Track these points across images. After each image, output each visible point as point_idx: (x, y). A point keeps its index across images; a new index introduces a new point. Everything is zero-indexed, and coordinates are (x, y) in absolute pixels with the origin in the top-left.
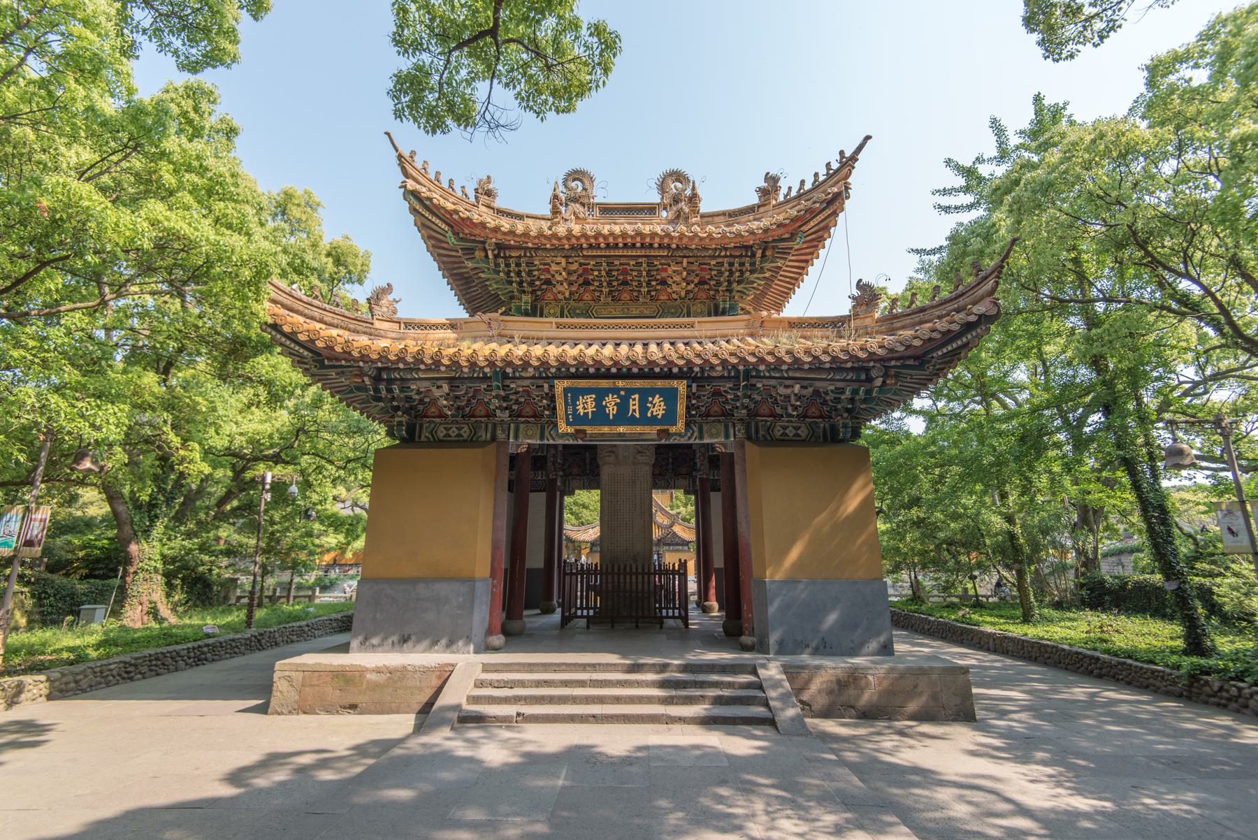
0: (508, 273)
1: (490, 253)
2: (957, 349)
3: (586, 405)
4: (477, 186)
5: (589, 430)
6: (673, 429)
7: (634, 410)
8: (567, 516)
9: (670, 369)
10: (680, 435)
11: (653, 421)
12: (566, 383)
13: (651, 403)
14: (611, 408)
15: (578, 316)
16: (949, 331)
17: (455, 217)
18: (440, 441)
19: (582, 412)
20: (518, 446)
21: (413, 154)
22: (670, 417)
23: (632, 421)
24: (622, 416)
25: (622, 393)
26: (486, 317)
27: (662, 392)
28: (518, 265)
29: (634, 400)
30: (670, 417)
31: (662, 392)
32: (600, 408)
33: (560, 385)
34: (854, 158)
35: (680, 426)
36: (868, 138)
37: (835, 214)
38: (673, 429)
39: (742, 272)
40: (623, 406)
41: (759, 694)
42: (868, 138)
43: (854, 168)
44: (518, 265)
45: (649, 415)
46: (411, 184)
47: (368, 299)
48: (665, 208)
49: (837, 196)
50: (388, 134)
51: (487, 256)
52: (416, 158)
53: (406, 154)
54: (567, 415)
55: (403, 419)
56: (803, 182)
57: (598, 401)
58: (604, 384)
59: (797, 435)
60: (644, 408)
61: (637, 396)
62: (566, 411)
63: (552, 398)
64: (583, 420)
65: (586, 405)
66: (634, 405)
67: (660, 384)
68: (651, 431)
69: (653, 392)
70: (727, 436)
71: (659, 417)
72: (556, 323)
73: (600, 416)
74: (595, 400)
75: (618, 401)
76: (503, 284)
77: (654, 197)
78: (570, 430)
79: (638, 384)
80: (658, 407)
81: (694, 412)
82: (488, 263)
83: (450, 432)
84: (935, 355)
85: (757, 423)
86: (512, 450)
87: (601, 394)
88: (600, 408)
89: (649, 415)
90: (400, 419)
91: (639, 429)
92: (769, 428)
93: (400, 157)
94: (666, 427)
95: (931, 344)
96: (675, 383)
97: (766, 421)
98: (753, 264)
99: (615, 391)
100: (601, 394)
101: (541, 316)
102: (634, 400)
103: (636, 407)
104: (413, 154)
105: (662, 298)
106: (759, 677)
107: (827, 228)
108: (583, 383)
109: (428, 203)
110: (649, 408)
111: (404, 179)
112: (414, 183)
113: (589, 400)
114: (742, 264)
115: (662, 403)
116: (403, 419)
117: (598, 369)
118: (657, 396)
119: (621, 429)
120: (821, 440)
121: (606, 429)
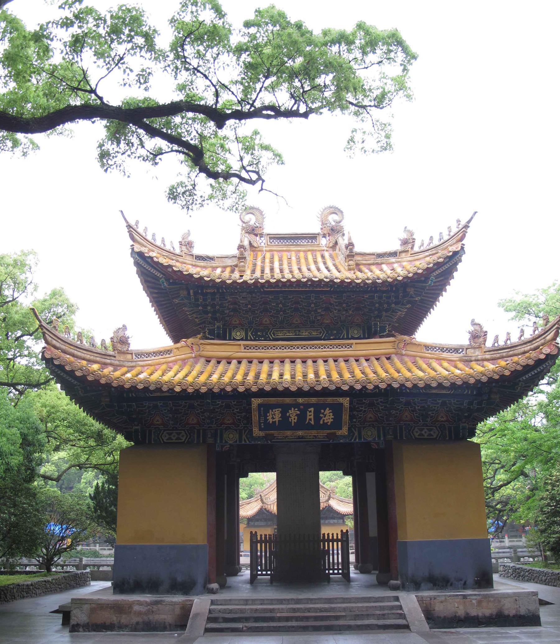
0: (205, 306)
1: (191, 292)
2: (536, 374)
3: (275, 416)
4: (181, 240)
5: (275, 433)
6: (339, 433)
7: (310, 419)
10: (344, 437)
11: (325, 426)
12: (260, 401)
13: (323, 414)
14: (293, 415)
16: (527, 365)
17: (170, 270)
19: (271, 421)
20: (222, 447)
21: (137, 223)
22: (337, 423)
23: (309, 427)
24: (302, 424)
25: (302, 407)
26: (190, 340)
27: (331, 406)
29: (310, 412)
30: (337, 423)
31: (331, 406)
32: (285, 417)
33: (256, 402)
34: (466, 226)
35: (344, 431)
36: (476, 212)
37: (456, 264)
38: (339, 433)
39: (389, 304)
40: (302, 416)
41: (397, 603)
42: (476, 212)
43: (467, 232)
44: (213, 299)
45: (321, 422)
46: (137, 248)
47: (112, 338)
48: (324, 236)
49: (455, 253)
50: (122, 212)
51: (189, 294)
52: (139, 225)
53: (132, 223)
54: (260, 423)
55: (138, 427)
56: (431, 238)
57: (284, 413)
58: (288, 400)
60: (317, 418)
61: (312, 409)
63: (249, 411)
64: (272, 427)
65: (275, 416)
66: (310, 415)
67: (329, 400)
68: (323, 433)
69: (324, 406)
71: (329, 424)
73: (285, 424)
74: (281, 412)
75: (298, 412)
77: (315, 228)
78: (262, 434)
79: (314, 400)
80: (328, 417)
81: (354, 420)
84: (521, 379)
86: (218, 449)
88: (285, 417)
89: (321, 422)
90: (137, 428)
91: (314, 432)
93: (129, 226)
94: (333, 431)
95: (516, 374)
96: (341, 400)
100: (285, 408)
102: (310, 412)
103: (312, 417)
104: (137, 223)
106: (407, 621)
109: (149, 260)
110: (322, 418)
111: (132, 243)
112: (139, 246)
113: (277, 412)
114: (389, 298)
115: (331, 414)
116: (138, 427)
119: (300, 433)
120: (447, 438)
121: (289, 433)
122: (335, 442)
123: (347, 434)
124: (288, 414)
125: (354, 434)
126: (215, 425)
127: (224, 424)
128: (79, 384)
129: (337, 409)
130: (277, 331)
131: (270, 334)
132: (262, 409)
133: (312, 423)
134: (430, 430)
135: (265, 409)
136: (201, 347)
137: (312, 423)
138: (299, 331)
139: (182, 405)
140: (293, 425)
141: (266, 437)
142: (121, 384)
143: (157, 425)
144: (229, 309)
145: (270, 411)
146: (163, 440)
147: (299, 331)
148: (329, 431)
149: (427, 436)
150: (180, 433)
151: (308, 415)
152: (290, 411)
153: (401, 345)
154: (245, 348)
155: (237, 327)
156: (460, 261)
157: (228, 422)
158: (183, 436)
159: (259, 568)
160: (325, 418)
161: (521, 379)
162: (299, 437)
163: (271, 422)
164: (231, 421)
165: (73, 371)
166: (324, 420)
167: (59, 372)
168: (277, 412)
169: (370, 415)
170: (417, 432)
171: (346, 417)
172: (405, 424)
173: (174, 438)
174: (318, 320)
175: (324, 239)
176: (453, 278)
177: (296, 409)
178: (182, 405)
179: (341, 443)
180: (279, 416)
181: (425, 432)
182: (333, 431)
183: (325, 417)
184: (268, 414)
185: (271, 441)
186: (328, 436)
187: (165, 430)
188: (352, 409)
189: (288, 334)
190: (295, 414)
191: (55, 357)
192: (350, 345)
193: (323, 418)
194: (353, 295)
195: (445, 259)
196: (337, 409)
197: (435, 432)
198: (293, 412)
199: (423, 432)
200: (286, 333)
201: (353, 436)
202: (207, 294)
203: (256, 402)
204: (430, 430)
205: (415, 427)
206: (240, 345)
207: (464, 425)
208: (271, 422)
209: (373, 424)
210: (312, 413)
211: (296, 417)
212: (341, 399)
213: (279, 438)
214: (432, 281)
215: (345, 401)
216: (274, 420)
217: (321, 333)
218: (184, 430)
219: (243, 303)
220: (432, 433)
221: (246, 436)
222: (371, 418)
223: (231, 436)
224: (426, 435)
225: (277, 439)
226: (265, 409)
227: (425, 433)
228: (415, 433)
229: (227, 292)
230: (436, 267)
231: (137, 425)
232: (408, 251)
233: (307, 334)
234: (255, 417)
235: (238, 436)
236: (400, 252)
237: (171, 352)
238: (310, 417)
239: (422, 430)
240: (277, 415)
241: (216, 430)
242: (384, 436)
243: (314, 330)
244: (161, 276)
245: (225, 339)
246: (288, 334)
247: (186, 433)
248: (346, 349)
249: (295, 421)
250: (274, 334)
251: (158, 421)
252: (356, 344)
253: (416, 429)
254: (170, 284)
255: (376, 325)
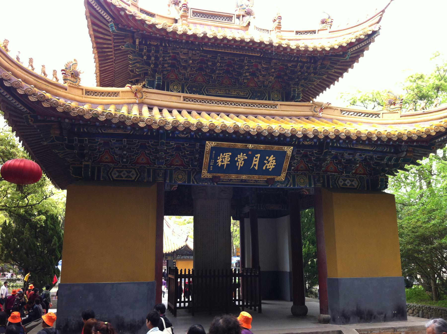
1: (137, 41)
6: (278, 178)
7: (255, 165)
8: (239, 226)
9: (224, 135)
10: (281, 182)
12: (213, 144)
14: (241, 159)
15: (194, 93)
17: (122, 13)
18: (114, 180)
20: (172, 186)
22: (277, 170)
23: (253, 172)
28: (157, 51)
29: (257, 157)
32: (233, 161)
33: (209, 145)
35: (282, 177)
38: (278, 178)
40: (248, 162)
44: (157, 51)
45: (264, 168)
51: (134, 42)
54: (209, 166)
57: (233, 158)
58: (239, 145)
59: (352, 185)
60: (261, 163)
62: (210, 163)
64: (221, 169)
66: (256, 161)
67: (276, 148)
68: (264, 178)
70: (310, 185)
71: (270, 170)
72: (184, 97)
75: (246, 158)
76: (143, 64)
78: (209, 176)
80: (271, 163)
82: (135, 48)
83: (122, 174)
85: (328, 177)
86: (167, 188)
87: (235, 153)
88: (233, 161)
89: (264, 168)
91: (256, 177)
92: (335, 180)
94: (272, 177)
97: (334, 175)
98: (315, 68)
99: (245, 151)
101: (168, 90)
102: (257, 157)
103: (257, 163)
105: (251, 85)
107: (362, 51)
108: (225, 144)
110: (265, 164)
115: (274, 161)
117: (224, 135)
118: (272, 156)
119: (244, 177)
120: (366, 189)
121: (233, 176)
122: (273, 187)
123: (284, 180)
124: (236, 159)
125: (289, 181)
126: (165, 166)
127: (173, 165)
128: (28, 111)
129: (280, 156)
130: (209, 88)
131: (204, 90)
132: (214, 152)
133: (256, 168)
134: (352, 181)
135: (217, 151)
136: (144, 95)
137: (256, 168)
138: (229, 91)
139: (135, 143)
140: (239, 169)
141: (213, 180)
142: (81, 114)
143: (106, 162)
144: (168, 63)
145: (221, 154)
146: (112, 177)
147: (229, 91)
148: (269, 177)
149: (350, 186)
150: (131, 171)
151: (254, 161)
152: (239, 156)
153: (318, 110)
154: (184, 100)
155: (174, 81)
156: (374, 41)
157: (177, 163)
158: (133, 174)
159: (179, 300)
160: (268, 165)
161: (437, 141)
162: (242, 181)
163: (220, 165)
164: (179, 163)
165: (26, 96)
166: (267, 166)
167: (8, 96)
168: (227, 156)
169: (302, 165)
170: (341, 182)
171: (286, 165)
172: (331, 175)
173: (124, 176)
174: (245, 83)
175: (238, 19)
176: (363, 56)
177: (245, 155)
178: (135, 143)
179: (278, 188)
180: (228, 160)
181: (348, 183)
182: (272, 177)
183: (268, 163)
184: (219, 158)
185: (217, 184)
186: (267, 181)
187: (114, 168)
188: (293, 157)
189: (220, 92)
190: (242, 159)
191: (5, 78)
192: (275, 106)
193: (266, 164)
194: (279, 63)
195: (365, 36)
196: (280, 156)
197: (355, 183)
198: (241, 157)
199: (346, 182)
200: (217, 91)
201: (288, 182)
202: (150, 45)
203: (209, 145)
204: (352, 181)
205: (339, 177)
206: (180, 96)
207: (382, 178)
208: (220, 165)
209: (305, 173)
210: (258, 159)
211: (243, 162)
212: (286, 147)
213: (225, 180)
214: (348, 55)
215: (289, 150)
216: (223, 164)
217: (247, 94)
218: (134, 169)
219: (182, 59)
220: (353, 183)
221: (194, 177)
222: (302, 167)
223: (180, 177)
224: (348, 185)
225: (223, 181)
226: (217, 151)
227: (348, 183)
228: (340, 183)
229: (169, 46)
230: (367, 37)
231: (88, 161)
232: (327, 29)
233: (235, 93)
234: (206, 160)
235: (186, 177)
236: (318, 31)
237: (118, 95)
238: (255, 163)
239: (345, 180)
240: (226, 159)
241: (166, 171)
242: (315, 184)
243: (241, 91)
244: (110, 20)
245: (163, 90)
246: (220, 92)
247: (136, 172)
248: (272, 109)
249: (242, 165)
250: (207, 90)
251: (107, 158)
252: (280, 105)
253: (341, 180)
254: (119, 29)
255: (294, 91)
